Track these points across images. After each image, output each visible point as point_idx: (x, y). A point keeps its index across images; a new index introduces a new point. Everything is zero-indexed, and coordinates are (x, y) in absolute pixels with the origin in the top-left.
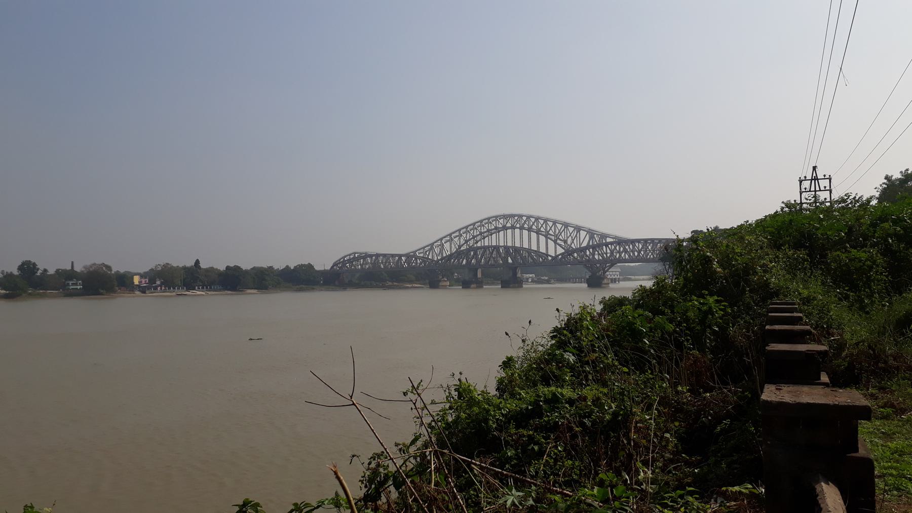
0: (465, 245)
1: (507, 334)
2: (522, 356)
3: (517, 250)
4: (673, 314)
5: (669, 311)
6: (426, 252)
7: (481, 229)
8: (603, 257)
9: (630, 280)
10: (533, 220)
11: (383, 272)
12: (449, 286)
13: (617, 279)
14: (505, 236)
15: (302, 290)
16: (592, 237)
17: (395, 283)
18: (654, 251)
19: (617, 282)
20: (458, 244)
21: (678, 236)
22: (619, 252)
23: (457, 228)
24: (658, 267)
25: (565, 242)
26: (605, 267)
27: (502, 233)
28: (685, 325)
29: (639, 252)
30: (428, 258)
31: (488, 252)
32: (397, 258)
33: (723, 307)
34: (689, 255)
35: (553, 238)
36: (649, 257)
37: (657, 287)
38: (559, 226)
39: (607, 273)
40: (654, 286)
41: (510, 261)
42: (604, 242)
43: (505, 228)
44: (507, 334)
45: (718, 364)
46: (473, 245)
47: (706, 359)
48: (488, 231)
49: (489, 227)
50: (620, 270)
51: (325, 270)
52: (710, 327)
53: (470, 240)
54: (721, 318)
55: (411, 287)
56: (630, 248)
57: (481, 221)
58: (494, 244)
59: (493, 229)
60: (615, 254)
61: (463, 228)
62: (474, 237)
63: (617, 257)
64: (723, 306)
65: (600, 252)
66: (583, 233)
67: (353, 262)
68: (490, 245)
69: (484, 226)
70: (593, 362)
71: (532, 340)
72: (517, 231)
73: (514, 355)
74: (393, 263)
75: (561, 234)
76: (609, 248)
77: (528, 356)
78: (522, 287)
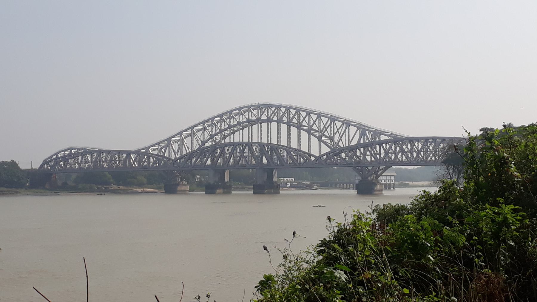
0: (211, 140)
1: (265, 248)
2: (283, 275)
3: (274, 148)
4: (462, 226)
5: (458, 222)
6: (162, 148)
7: (230, 122)
8: (375, 158)
9: (407, 186)
10: (293, 112)
11: (107, 173)
12: (189, 191)
13: (392, 185)
14: (260, 131)
15: (3, 194)
16: (363, 135)
17: (121, 187)
18: (436, 151)
19: (392, 189)
20: (202, 140)
21: (469, 134)
22: (395, 153)
23: (190, 125)
24: (441, 171)
25: (332, 139)
26: (378, 171)
27: (255, 127)
28: (477, 238)
29: (418, 153)
30: (163, 156)
31: (238, 150)
32: (125, 155)
33: (520, 218)
34: (482, 155)
35: (317, 134)
36: (429, 158)
37: (444, 193)
38: (325, 120)
39: (381, 178)
40: (439, 191)
41: (265, 161)
42: (377, 139)
43: (259, 121)
44: (265, 248)
45: (514, 286)
46: (220, 141)
47: (500, 280)
48: (239, 124)
49: (239, 119)
50: (395, 174)
51: (32, 168)
52: (505, 241)
53: (216, 134)
54: (517, 230)
55: (142, 192)
56: (408, 148)
57: (231, 112)
58: (246, 140)
59: (245, 122)
60: (390, 155)
61: (208, 120)
62: (221, 131)
63: (393, 158)
64: (520, 216)
65: (372, 153)
66: (353, 129)
67: (68, 160)
68: (241, 141)
69: (234, 118)
70: (368, 281)
71: (296, 254)
72: (274, 125)
73: (274, 274)
74: (119, 161)
75: (326, 130)
76: (383, 147)
77: (290, 276)
78: (279, 193)
